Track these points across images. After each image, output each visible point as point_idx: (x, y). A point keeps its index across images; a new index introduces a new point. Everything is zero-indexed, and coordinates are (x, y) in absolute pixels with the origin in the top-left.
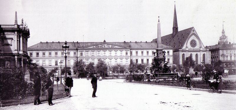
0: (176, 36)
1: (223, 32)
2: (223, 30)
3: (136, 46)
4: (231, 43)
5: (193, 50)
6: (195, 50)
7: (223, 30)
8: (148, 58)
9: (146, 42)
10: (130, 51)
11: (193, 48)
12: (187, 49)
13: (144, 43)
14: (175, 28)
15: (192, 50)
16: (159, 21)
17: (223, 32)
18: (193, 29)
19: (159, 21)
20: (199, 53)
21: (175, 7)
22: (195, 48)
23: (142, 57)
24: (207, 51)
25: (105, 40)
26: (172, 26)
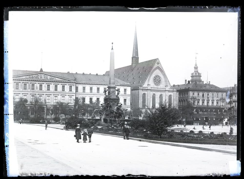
1: (196, 68)
2: (196, 65)
5: (156, 89)
6: (159, 89)
7: (196, 65)
10: (75, 86)
11: (156, 87)
14: (135, 58)
17: (196, 68)
20: (164, 94)
25: (41, 69)
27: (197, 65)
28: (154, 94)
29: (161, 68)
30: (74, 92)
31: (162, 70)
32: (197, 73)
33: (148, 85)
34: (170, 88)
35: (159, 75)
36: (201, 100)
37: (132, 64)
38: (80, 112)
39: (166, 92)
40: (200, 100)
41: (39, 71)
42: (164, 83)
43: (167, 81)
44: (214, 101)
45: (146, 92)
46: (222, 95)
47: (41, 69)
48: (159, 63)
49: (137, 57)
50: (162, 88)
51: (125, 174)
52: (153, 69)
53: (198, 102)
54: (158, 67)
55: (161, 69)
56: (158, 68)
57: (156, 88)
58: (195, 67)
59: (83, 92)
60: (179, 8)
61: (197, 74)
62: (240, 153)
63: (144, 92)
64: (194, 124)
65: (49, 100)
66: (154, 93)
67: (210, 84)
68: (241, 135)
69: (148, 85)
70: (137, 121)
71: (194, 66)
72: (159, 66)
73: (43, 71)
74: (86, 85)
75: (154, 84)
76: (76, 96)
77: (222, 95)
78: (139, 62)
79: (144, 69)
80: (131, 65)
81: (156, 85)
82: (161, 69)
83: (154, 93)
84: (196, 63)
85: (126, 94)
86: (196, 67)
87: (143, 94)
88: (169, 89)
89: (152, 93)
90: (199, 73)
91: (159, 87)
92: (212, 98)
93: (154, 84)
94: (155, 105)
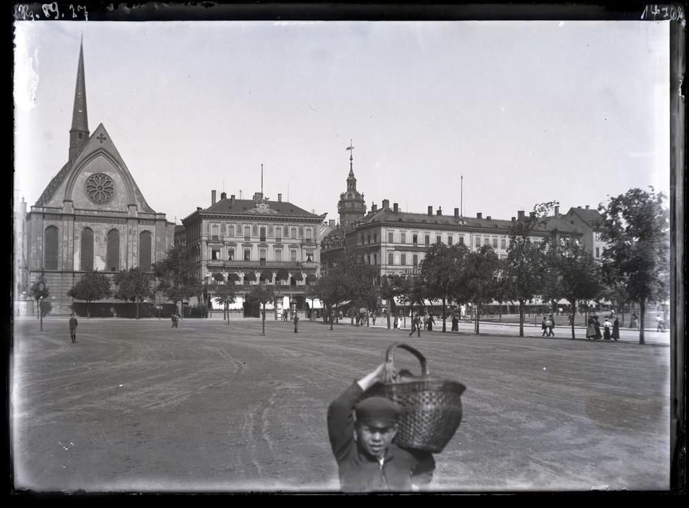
1: (351, 182)
2: (351, 175)
6: (104, 214)
7: (351, 175)
11: (93, 206)
17: (351, 182)
27: (353, 175)
28: (87, 228)
29: (112, 154)
31: (116, 157)
33: (64, 201)
34: (144, 212)
35: (108, 174)
36: (239, 245)
39: (129, 221)
42: (123, 196)
44: (251, 246)
45: (58, 223)
46: (403, 235)
48: (105, 139)
50: (117, 210)
52: (85, 156)
54: (101, 149)
55: (112, 157)
56: (101, 152)
57: (82, 211)
58: (348, 180)
60: (194, 7)
61: (354, 196)
62: (664, 275)
64: (209, 314)
66: (89, 224)
67: (282, 201)
68: (17, 415)
69: (64, 201)
72: (103, 148)
75: (87, 200)
77: (403, 235)
81: (95, 202)
82: (112, 157)
83: (89, 224)
84: (351, 170)
86: (352, 179)
87: (45, 227)
88: (138, 213)
89: (79, 226)
90: (358, 194)
91: (108, 209)
92: (244, 239)
93: (87, 200)
94: (91, 262)
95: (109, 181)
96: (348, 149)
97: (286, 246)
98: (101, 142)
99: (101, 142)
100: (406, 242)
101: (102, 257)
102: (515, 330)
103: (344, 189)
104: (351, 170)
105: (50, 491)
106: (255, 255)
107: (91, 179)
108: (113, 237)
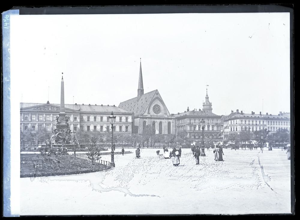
0: (141, 99)
1: (207, 98)
2: (207, 95)
3: (89, 110)
4: (283, 112)
5: (156, 117)
6: (158, 117)
7: (207, 95)
8: (88, 124)
9: (102, 105)
10: (79, 116)
11: (155, 115)
12: (149, 116)
13: (87, 106)
14: (141, 91)
15: (154, 117)
16: (62, 78)
17: (207, 98)
18: (157, 92)
19: (62, 78)
20: (163, 121)
21: (141, 65)
22: (159, 115)
23: (120, 123)
24: (172, 118)
25: (48, 101)
26: (136, 87)
28: (154, 121)
30: (79, 121)
32: (208, 102)
35: (159, 104)
37: (138, 95)
38: (160, 139)
40: (196, 126)
41: (47, 103)
43: (166, 109)
45: (162, 121)
47: (48, 101)
49: (142, 89)
51: (204, 214)
53: (195, 128)
58: (206, 98)
59: (107, 121)
63: (145, 120)
65: (49, 129)
70: (60, 154)
71: (205, 96)
73: (50, 103)
74: (90, 115)
76: (80, 124)
78: (144, 93)
79: (146, 100)
80: (137, 96)
81: (155, 113)
84: (207, 94)
85: (121, 122)
89: (167, 121)
95: (159, 107)
96: (208, 86)
97: (211, 126)
98: (157, 95)
99: (157, 95)
100: (90, 121)
101: (158, 130)
102: (76, 153)
103: (205, 101)
104: (207, 94)
105: (3, 190)
106: (255, 130)
107: (154, 106)
108: (161, 123)
